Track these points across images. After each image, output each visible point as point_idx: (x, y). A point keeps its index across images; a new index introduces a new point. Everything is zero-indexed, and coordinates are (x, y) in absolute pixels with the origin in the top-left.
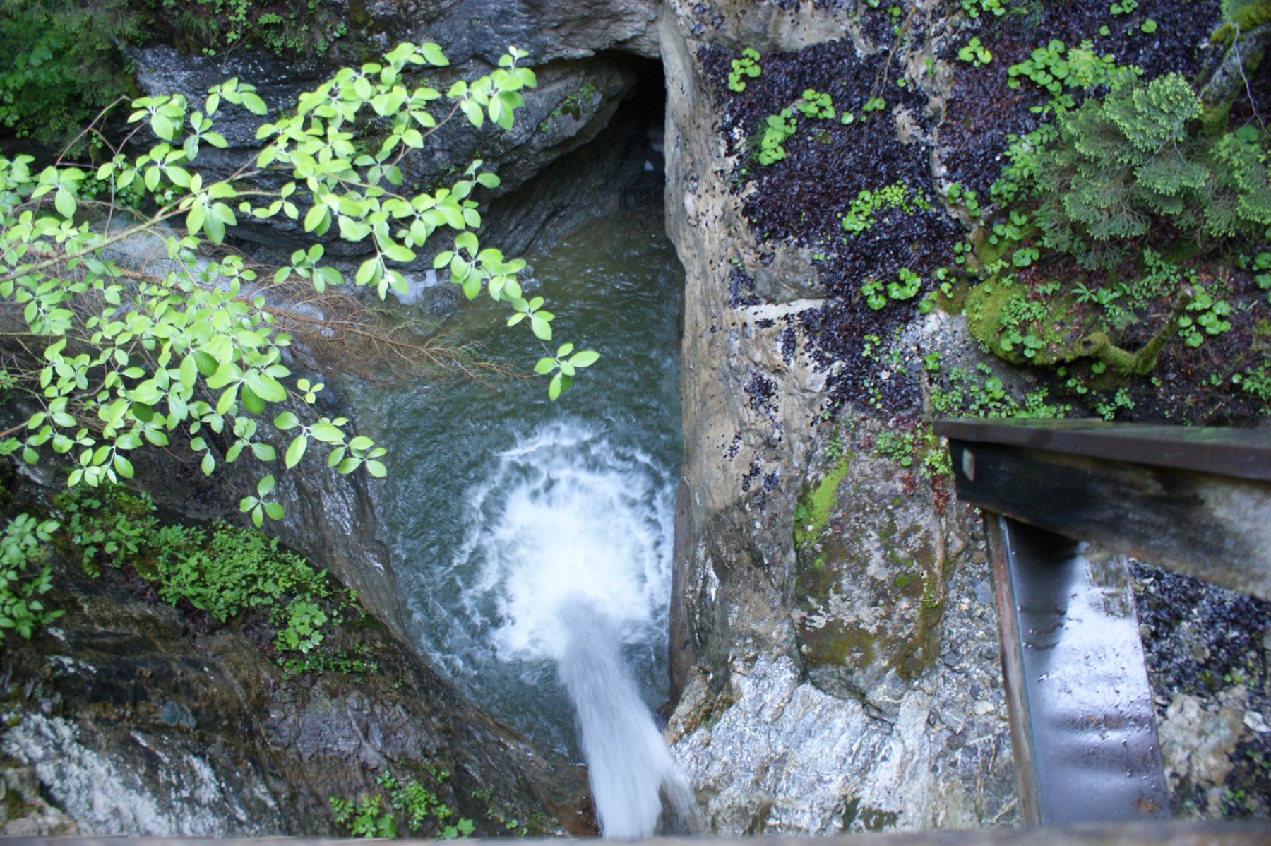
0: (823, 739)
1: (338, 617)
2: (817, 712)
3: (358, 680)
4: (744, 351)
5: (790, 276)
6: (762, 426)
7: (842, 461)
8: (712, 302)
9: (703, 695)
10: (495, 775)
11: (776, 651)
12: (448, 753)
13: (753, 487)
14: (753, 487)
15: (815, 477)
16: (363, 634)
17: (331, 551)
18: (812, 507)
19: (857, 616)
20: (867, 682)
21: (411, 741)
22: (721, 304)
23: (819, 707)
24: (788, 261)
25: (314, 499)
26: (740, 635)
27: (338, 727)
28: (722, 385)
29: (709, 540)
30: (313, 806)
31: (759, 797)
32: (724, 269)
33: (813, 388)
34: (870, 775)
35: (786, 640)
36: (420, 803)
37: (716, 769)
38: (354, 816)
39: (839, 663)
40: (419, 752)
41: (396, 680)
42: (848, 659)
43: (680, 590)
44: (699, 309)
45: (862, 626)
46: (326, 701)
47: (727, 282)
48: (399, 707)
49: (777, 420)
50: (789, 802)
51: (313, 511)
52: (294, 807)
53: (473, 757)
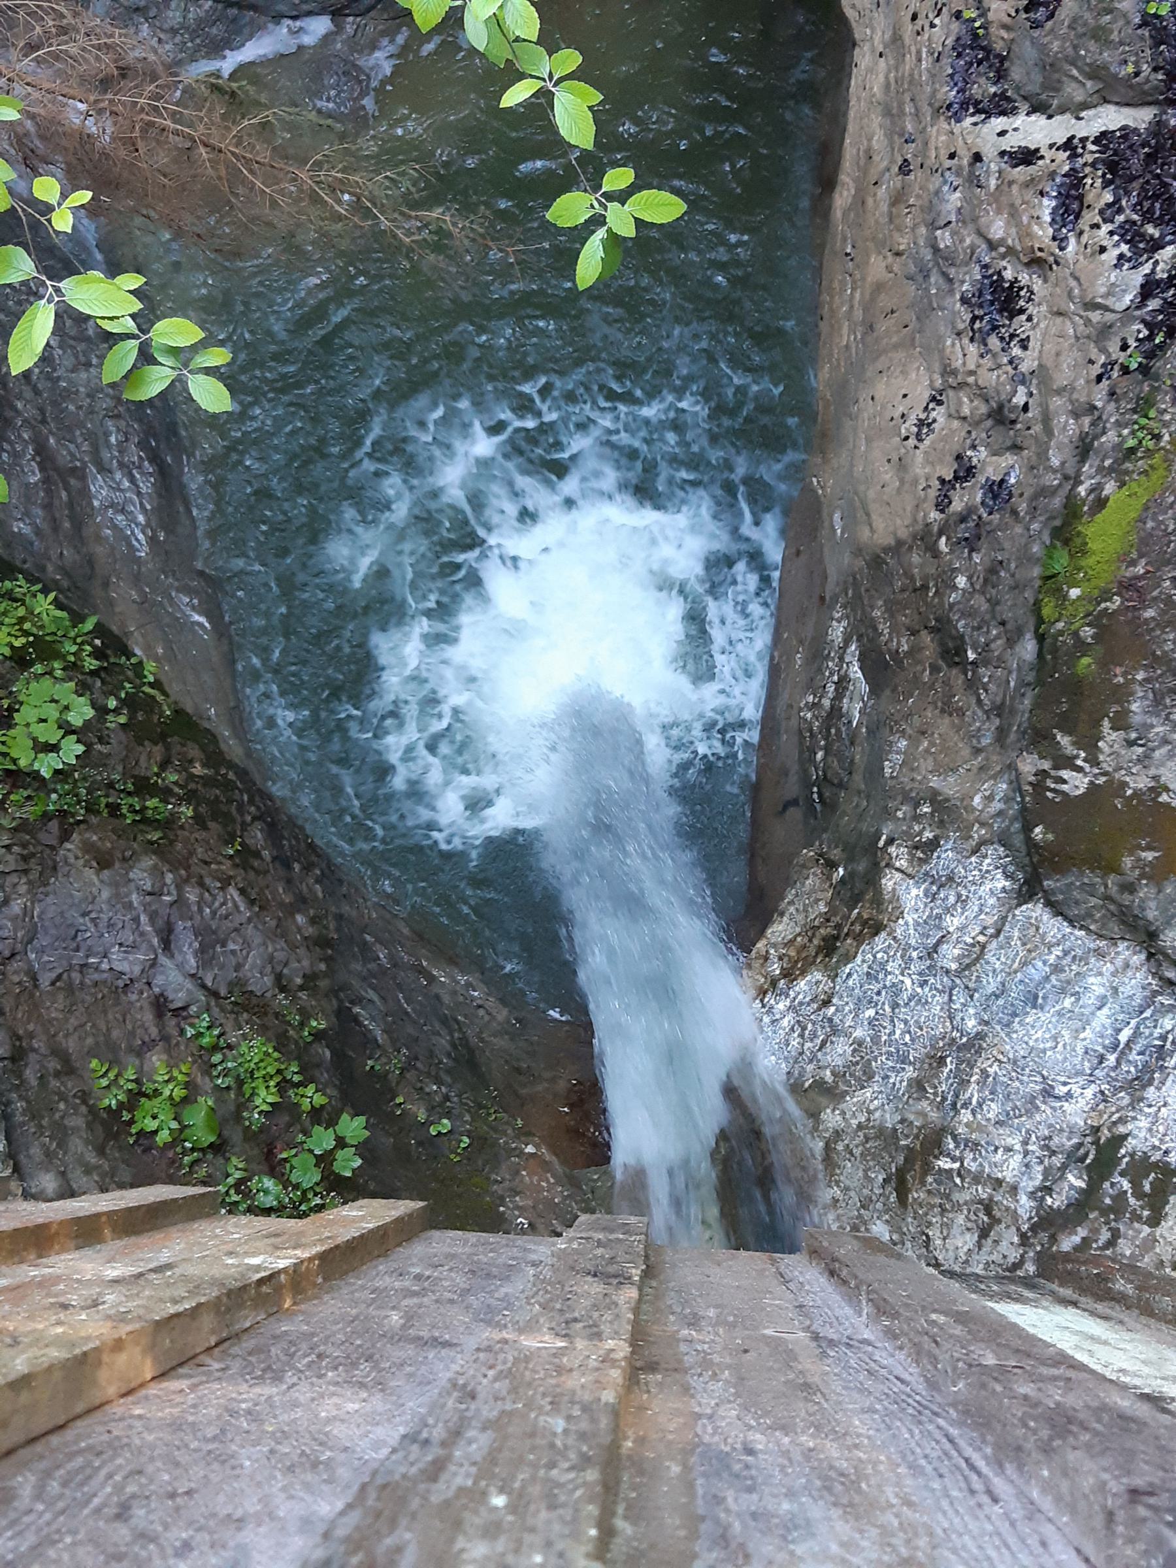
0: (1060, 1014)
1: (116, 711)
2: (1052, 959)
3: (155, 836)
4: (969, 217)
5: (1090, 51)
6: (989, 379)
7: (1157, 459)
8: (909, 108)
9: (822, 908)
10: (411, 1030)
11: (979, 832)
12: (323, 984)
13: (957, 506)
14: (957, 506)
15: (1096, 489)
16: (168, 748)
17: (106, 584)
18: (1084, 551)
19: (1155, 778)
20: (1164, 910)
21: (254, 958)
22: (927, 112)
23: (1057, 951)
24: (1087, 16)
25: (73, 482)
26: (906, 798)
27: (110, 925)
28: (911, 289)
29: (857, 607)
30: (57, 1074)
31: (924, 1115)
32: (943, 32)
33: (1109, 302)
34: (1151, 1092)
35: (1000, 813)
36: (267, 1078)
37: (839, 1052)
38: (136, 1096)
39: (1113, 868)
40: (268, 980)
41: (230, 841)
42: (1128, 862)
43: (785, 697)
44: (876, 121)
45: (1164, 798)
46: (90, 874)
47: (945, 61)
48: (233, 892)
49: (1024, 368)
50: (980, 1128)
51: (71, 505)
52: (20, 1076)
53: (372, 994)
